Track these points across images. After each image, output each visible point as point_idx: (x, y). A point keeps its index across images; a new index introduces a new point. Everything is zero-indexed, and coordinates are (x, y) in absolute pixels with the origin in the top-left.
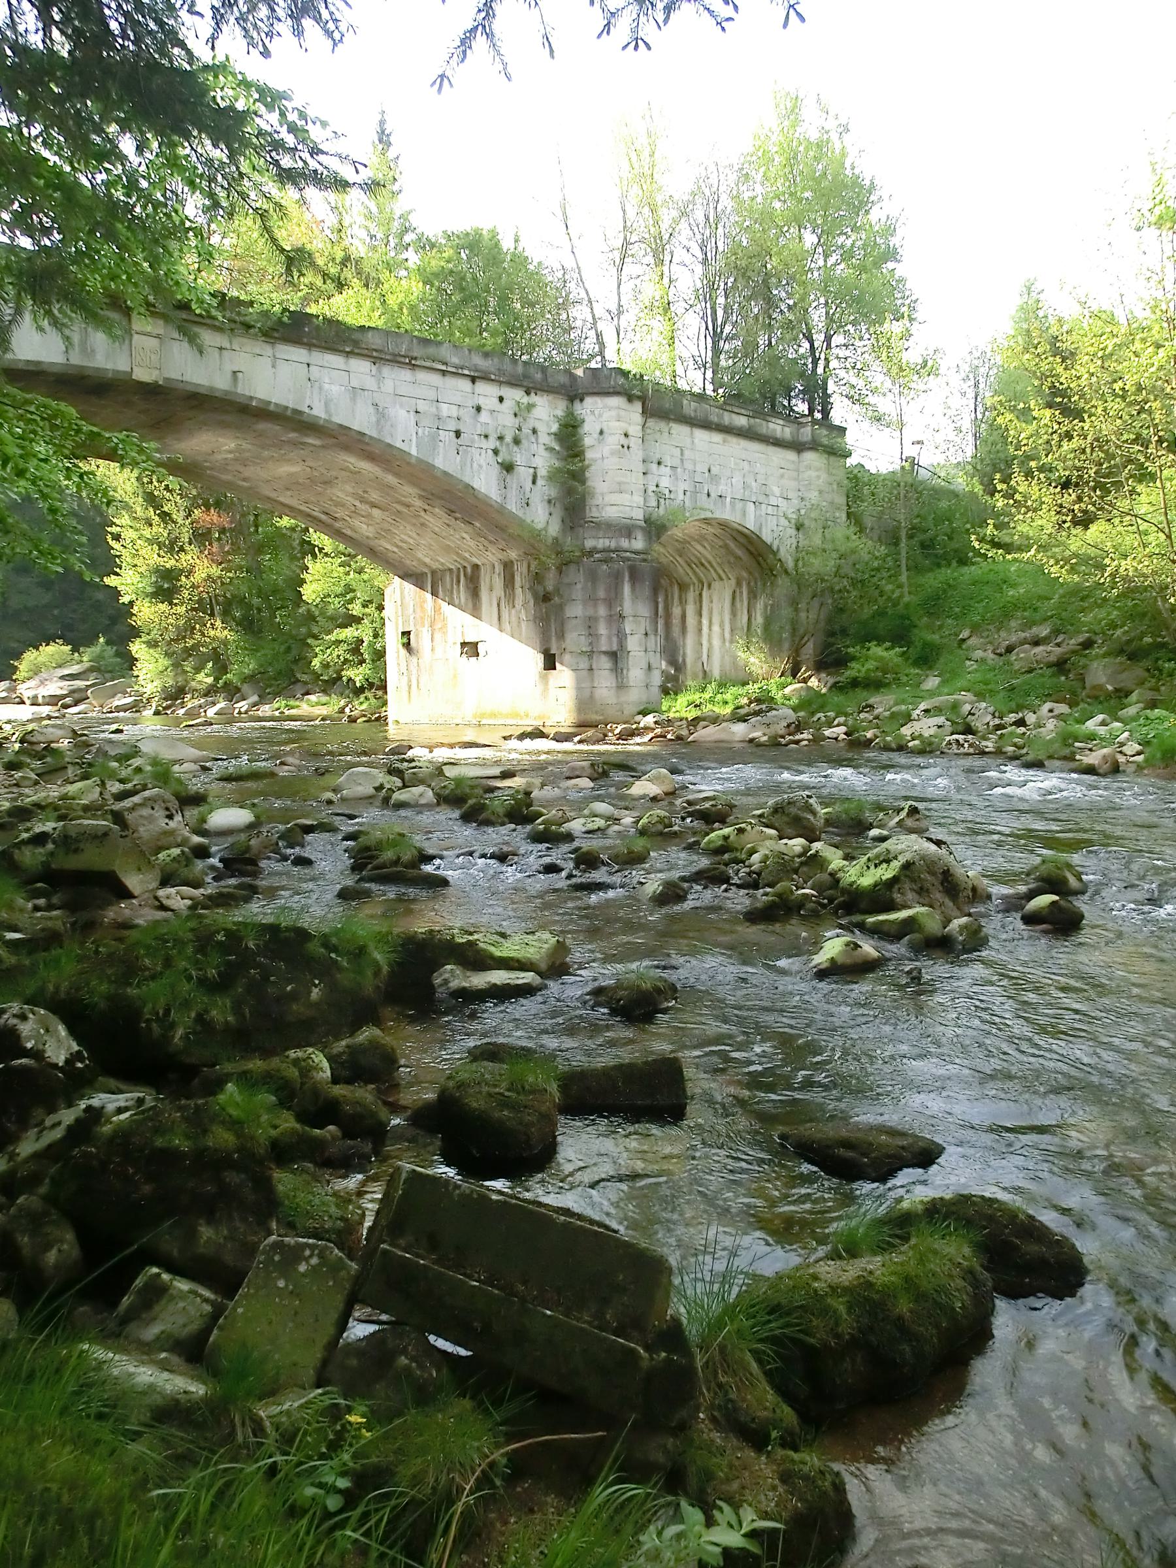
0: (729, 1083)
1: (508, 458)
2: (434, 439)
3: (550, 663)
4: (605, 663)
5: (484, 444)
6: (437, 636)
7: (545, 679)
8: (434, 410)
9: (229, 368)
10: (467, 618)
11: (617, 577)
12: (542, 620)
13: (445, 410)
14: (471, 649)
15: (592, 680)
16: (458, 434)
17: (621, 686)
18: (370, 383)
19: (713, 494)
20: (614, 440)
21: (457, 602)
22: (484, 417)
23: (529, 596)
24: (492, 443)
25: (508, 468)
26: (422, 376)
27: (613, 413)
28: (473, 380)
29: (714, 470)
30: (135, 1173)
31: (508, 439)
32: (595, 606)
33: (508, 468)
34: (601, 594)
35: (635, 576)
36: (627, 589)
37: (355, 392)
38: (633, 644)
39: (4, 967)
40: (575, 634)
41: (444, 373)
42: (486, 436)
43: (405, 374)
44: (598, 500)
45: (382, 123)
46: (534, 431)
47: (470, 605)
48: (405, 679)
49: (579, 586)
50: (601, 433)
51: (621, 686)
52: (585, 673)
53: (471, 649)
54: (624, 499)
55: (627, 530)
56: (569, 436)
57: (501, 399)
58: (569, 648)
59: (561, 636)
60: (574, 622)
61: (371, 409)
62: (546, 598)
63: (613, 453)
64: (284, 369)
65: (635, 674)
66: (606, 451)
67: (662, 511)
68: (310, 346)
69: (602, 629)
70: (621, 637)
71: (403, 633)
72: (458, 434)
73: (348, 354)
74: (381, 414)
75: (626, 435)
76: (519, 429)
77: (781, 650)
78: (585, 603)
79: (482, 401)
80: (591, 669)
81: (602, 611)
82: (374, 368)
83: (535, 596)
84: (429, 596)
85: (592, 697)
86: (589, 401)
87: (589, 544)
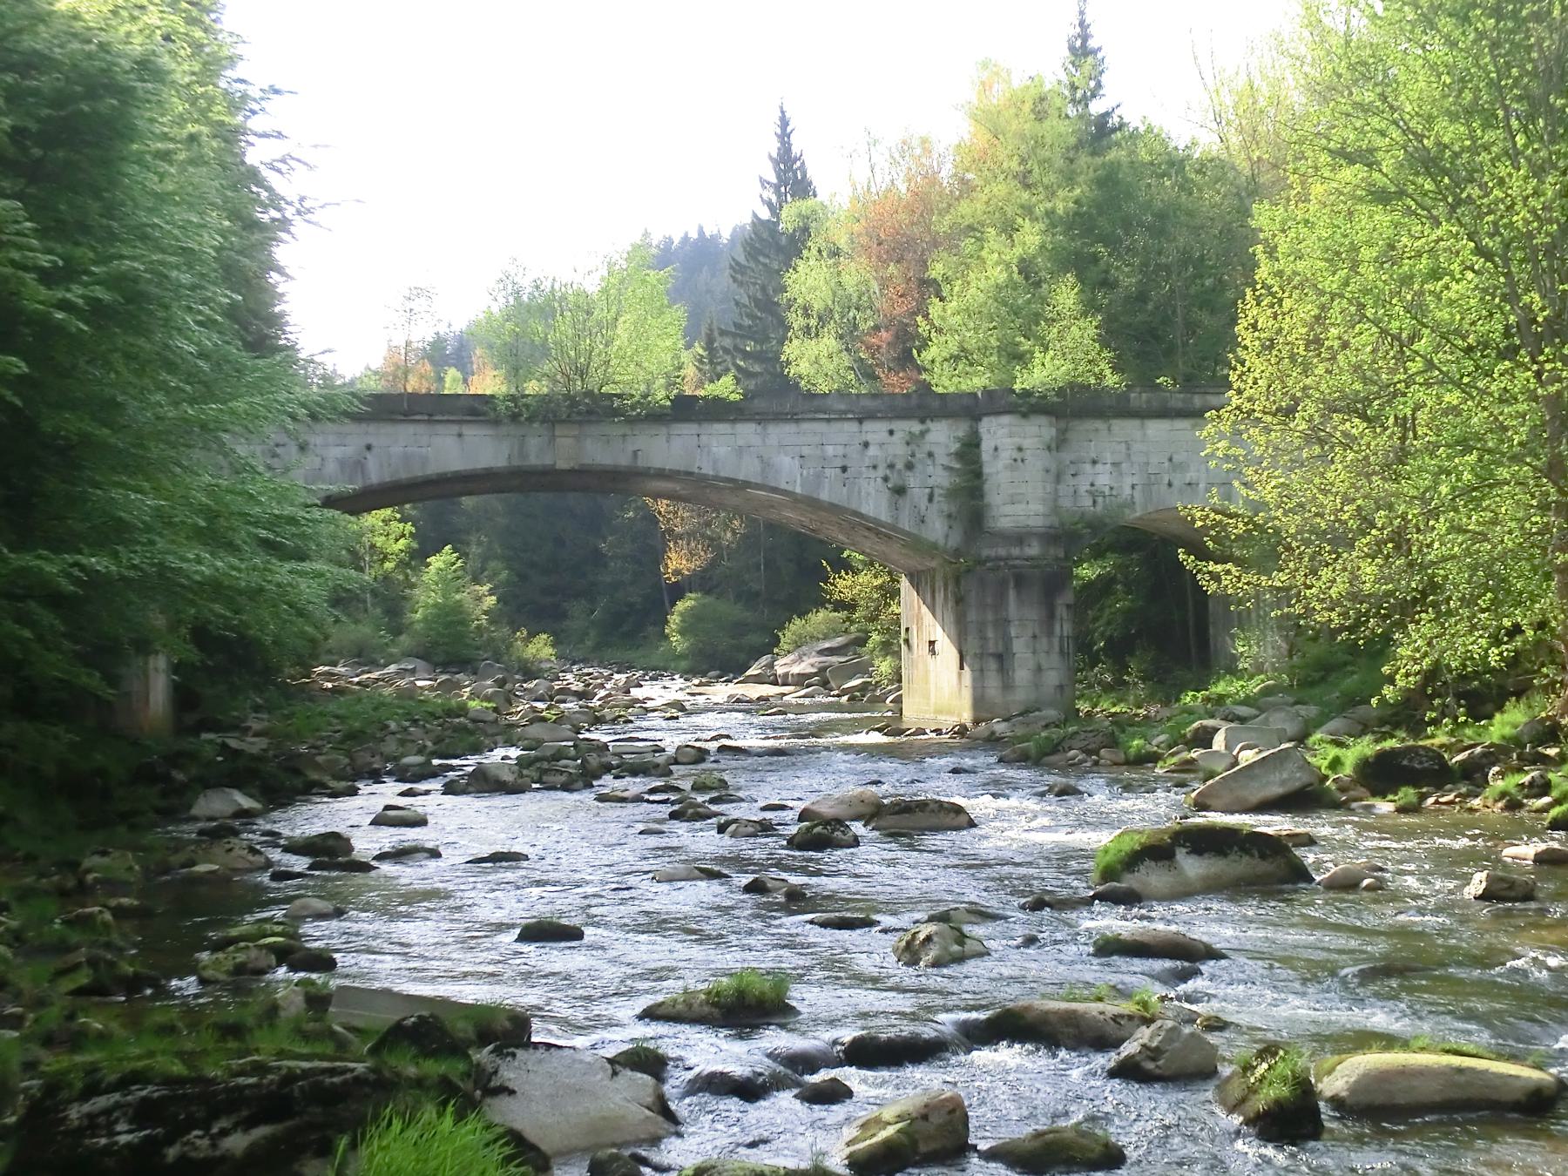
1: (900, 483)
2: (819, 477)
4: (992, 665)
5: (872, 474)
8: (819, 452)
9: (630, 448)
11: (1002, 587)
13: (830, 450)
16: (844, 469)
17: (1007, 686)
18: (756, 440)
19: (1176, 483)
20: (1006, 455)
22: (872, 451)
24: (881, 472)
25: (900, 491)
26: (805, 426)
27: (1005, 431)
28: (860, 421)
29: (1176, 458)
30: (1383, 701)
31: (900, 465)
33: (900, 491)
34: (989, 601)
35: (1020, 581)
36: (1012, 594)
37: (740, 451)
38: (1019, 647)
41: (828, 420)
42: (875, 467)
43: (790, 428)
44: (994, 512)
46: (930, 455)
50: (996, 449)
51: (1007, 686)
54: (1019, 509)
55: (1020, 538)
56: (969, 451)
57: (891, 432)
61: (756, 461)
63: (1006, 467)
64: (677, 443)
65: (1022, 675)
66: (1000, 465)
67: (1099, 508)
68: (699, 421)
69: (990, 634)
70: (1007, 641)
72: (844, 469)
73: (734, 421)
74: (765, 463)
75: (1020, 449)
76: (913, 455)
77: (269, 983)
79: (869, 437)
81: (990, 616)
82: (759, 428)
86: (985, 420)
87: (986, 552)
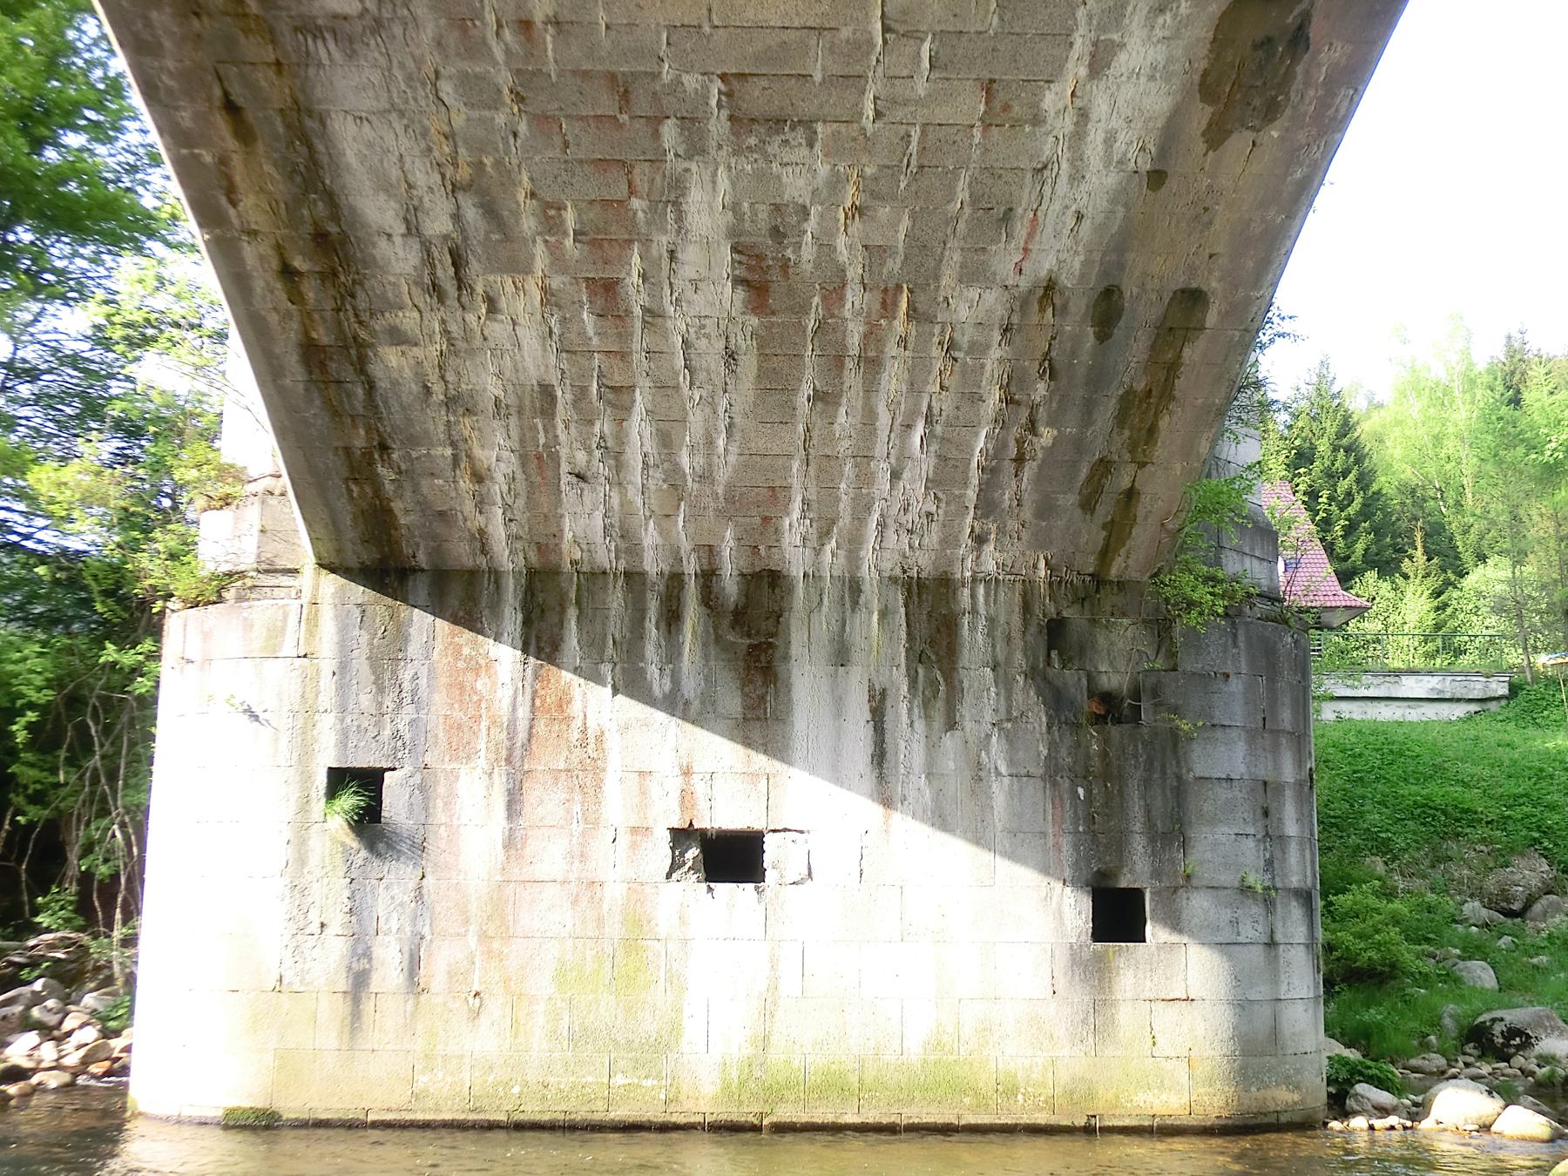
0: (114, 791)
3: (1117, 917)
6: (544, 801)
7: (1096, 975)
10: (716, 752)
12: (1083, 775)
14: (731, 857)
15: (1275, 981)
21: (659, 683)
23: (1027, 697)
32: (1275, 750)
39: (31, 1122)
40: (1224, 833)
45: (356, 1015)
47: (732, 702)
48: (335, 949)
49: (1236, 686)
52: (1257, 954)
53: (731, 857)
58: (1205, 875)
59: (1172, 834)
60: (1223, 793)
62: (1112, 709)
71: (339, 779)
78: (1252, 736)
80: (1272, 944)
83: (1056, 701)
84: (505, 657)
85: (1275, 1033)
